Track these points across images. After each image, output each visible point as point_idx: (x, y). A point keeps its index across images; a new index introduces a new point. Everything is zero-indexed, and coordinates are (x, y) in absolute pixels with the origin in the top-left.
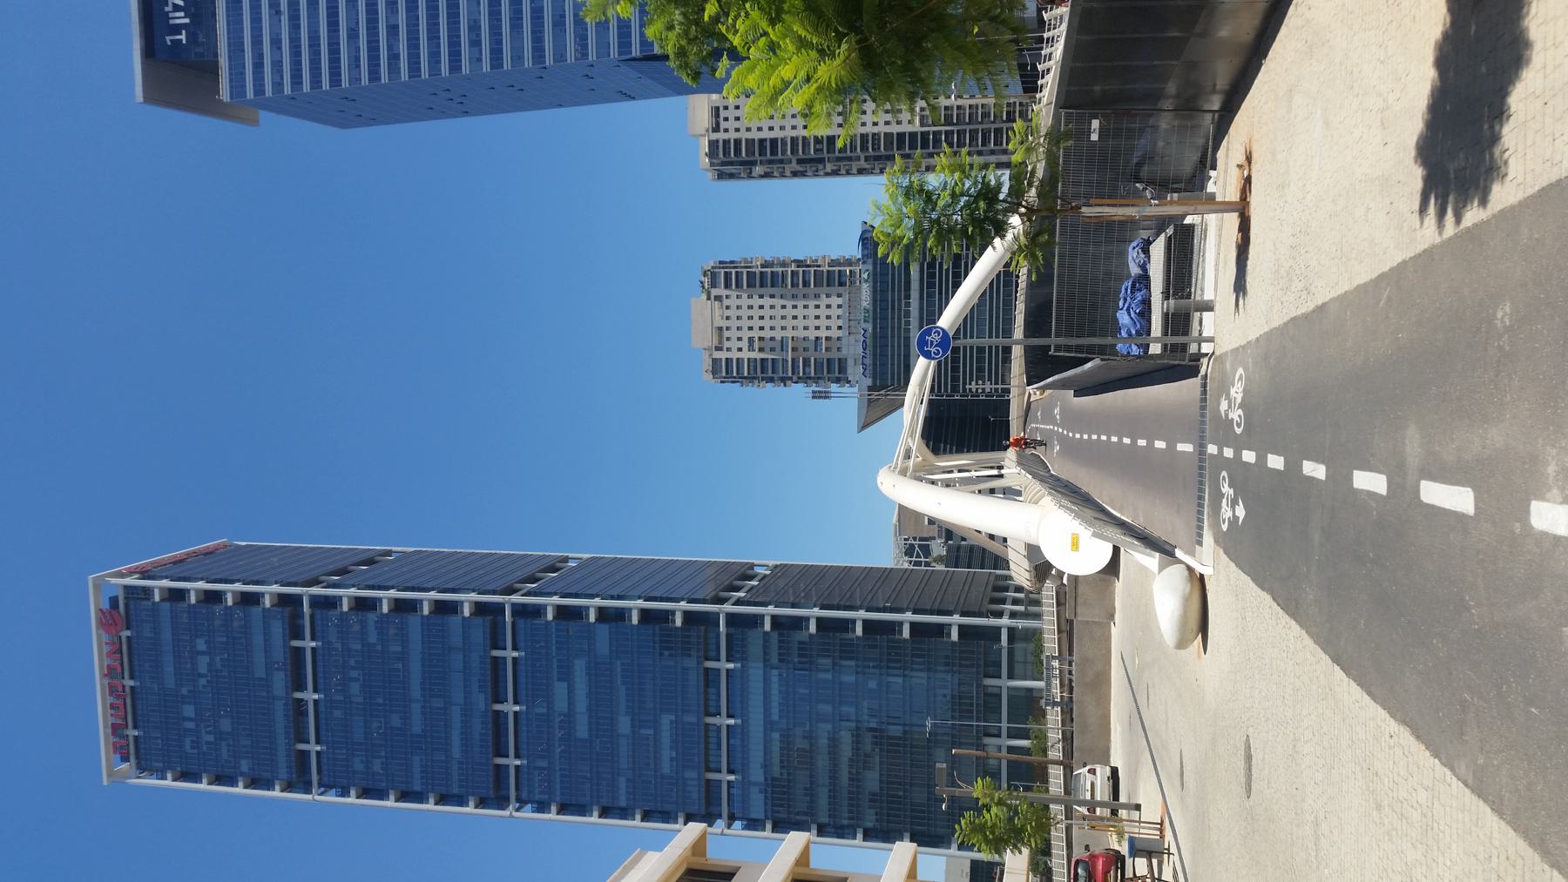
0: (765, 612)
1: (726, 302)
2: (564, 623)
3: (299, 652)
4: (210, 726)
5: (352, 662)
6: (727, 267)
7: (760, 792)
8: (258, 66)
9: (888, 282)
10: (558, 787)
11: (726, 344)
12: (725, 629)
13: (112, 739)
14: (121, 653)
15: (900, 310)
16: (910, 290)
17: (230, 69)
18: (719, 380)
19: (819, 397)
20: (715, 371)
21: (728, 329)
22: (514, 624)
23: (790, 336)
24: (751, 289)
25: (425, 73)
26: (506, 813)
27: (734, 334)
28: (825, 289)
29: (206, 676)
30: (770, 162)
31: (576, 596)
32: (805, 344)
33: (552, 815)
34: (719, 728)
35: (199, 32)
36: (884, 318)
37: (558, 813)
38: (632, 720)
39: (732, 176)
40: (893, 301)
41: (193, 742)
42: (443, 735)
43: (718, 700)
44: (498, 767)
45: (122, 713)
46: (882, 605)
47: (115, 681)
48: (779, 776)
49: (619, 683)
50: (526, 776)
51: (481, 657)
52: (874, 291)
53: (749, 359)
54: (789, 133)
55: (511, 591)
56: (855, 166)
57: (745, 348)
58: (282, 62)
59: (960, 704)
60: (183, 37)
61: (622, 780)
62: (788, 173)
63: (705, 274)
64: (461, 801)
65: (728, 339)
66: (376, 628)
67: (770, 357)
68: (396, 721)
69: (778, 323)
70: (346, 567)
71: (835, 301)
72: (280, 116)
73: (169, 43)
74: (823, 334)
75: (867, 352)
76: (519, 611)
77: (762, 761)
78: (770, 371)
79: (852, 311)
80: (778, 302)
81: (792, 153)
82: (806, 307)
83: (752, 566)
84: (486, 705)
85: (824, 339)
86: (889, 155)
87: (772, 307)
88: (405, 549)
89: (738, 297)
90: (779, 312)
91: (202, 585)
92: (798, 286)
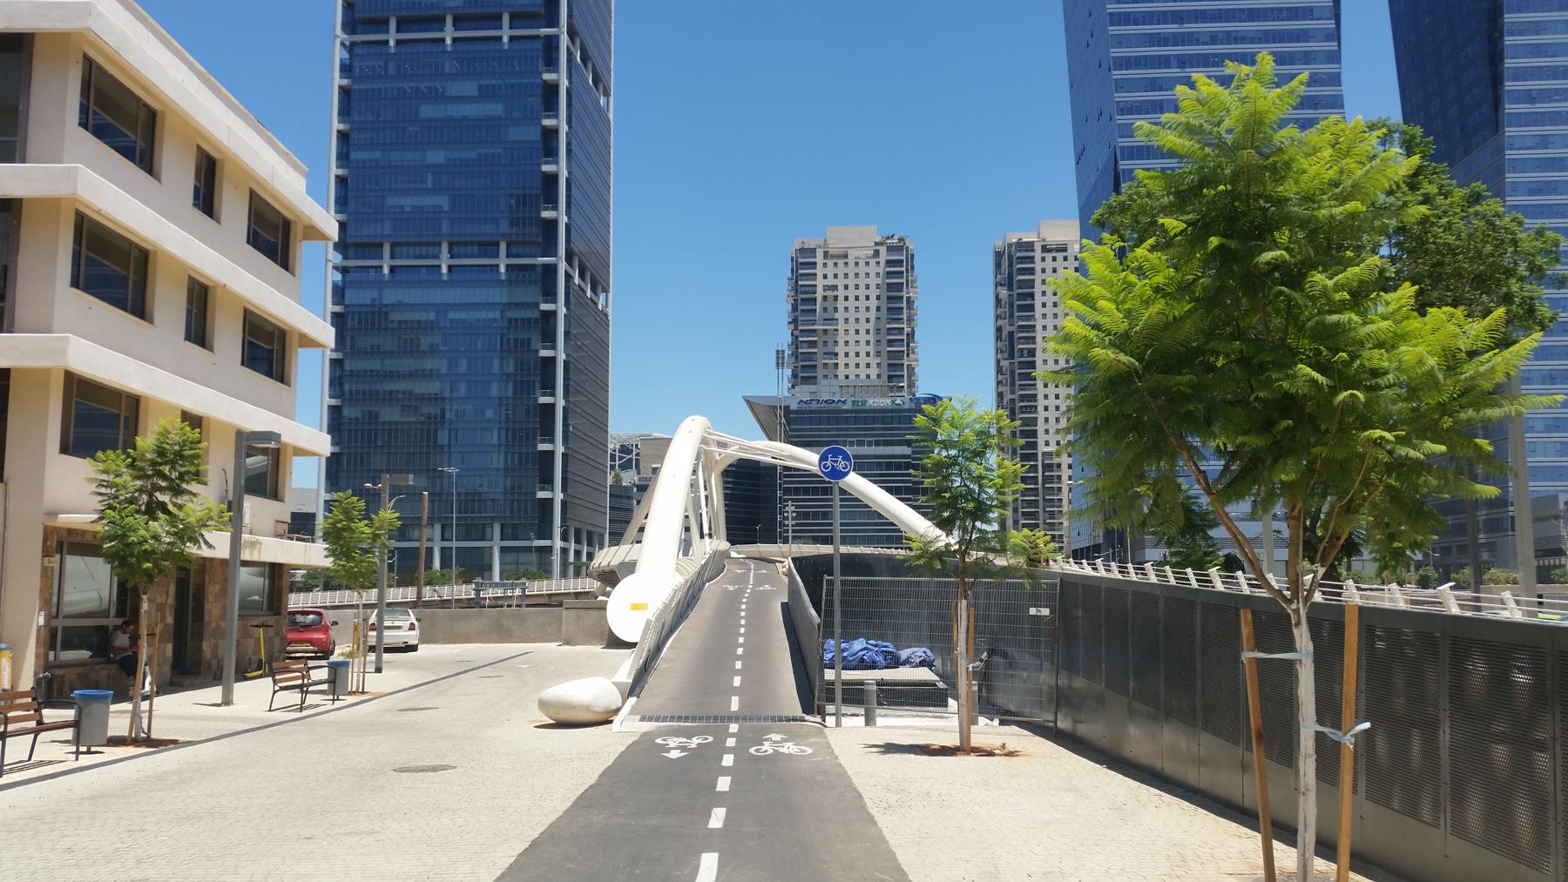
0: (559, 304)
1: (873, 262)
2: (540, 92)
6: (907, 262)
11: (830, 263)
15: (865, 436)
19: (778, 358)
20: (803, 251)
21: (846, 264)
22: (537, 37)
23: (839, 328)
26: (339, 31)
27: (841, 270)
28: (885, 362)
30: (1011, 305)
31: (569, 105)
32: (831, 343)
33: (338, 81)
34: (436, 257)
38: (441, 165)
39: (998, 265)
43: (467, 256)
44: (386, 22)
49: (480, 151)
52: (883, 411)
55: (572, 34)
56: (1005, 389)
59: (473, 501)
61: (377, 155)
62: (1000, 322)
63: (901, 240)
65: (836, 264)
67: (818, 307)
71: (874, 372)
74: (841, 361)
75: (824, 405)
79: (871, 389)
80: (873, 315)
82: (868, 343)
83: (606, 290)
84: (451, 8)
87: (868, 309)
89: (878, 274)
90: (863, 316)
92: (888, 334)
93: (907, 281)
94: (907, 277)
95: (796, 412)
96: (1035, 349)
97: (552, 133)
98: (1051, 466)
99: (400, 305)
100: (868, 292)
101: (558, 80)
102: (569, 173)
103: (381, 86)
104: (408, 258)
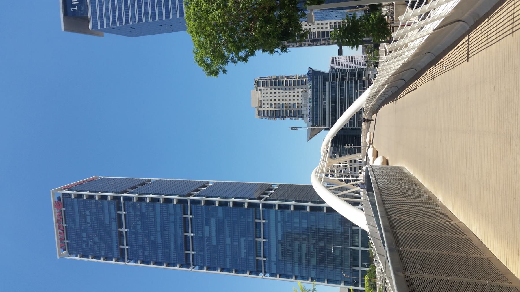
0: (276, 203)
1: (263, 91)
2: (208, 206)
3: (120, 215)
4: (91, 240)
5: (137, 219)
6: (263, 79)
7: (275, 264)
8: (102, 17)
10: (206, 261)
11: (263, 106)
12: (262, 209)
13: (60, 244)
14: (62, 215)
15: (322, 98)
17: (92, 19)
19: (294, 129)
21: (263, 100)
22: (191, 206)
23: (285, 103)
25: (157, 19)
26: (189, 269)
27: (265, 102)
29: (89, 223)
32: (290, 105)
33: (205, 271)
34: (260, 242)
35: (82, 7)
36: (316, 101)
37: (207, 270)
38: (231, 239)
40: (319, 95)
41: (86, 245)
42: (168, 241)
43: (260, 233)
44: (187, 254)
45: (63, 235)
46: (316, 201)
47: (61, 225)
48: (281, 259)
49: (226, 226)
50: (196, 259)
51: (180, 217)
52: (313, 92)
53: (271, 111)
55: (189, 195)
56: (307, 43)
58: (109, 16)
59: (344, 235)
60: (76, 8)
61: (228, 259)
63: (255, 82)
64: (175, 265)
65: (264, 104)
66: (145, 207)
67: (278, 110)
68: (152, 238)
69: (281, 98)
70: (136, 186)
72: (110, 34)
73: (72, 11)
74: (296, 102)
75: (310, 113)
76: (192, 202)
79: (305, 99)
80: (281, 91)
82: (290, 92)
83: (271, 185)
84: (182, 234)
85: (296, 103)
87: (279, 93)
88: (155, 179)
89: (267, 90)
90: (281, 94)
91: (87, 193)
93: (269, 79)
94: (268, 79)
95: (313, 123)
97: (220, 203)
101: (204, 200)
102: (233, 198)
103: (206, 257)
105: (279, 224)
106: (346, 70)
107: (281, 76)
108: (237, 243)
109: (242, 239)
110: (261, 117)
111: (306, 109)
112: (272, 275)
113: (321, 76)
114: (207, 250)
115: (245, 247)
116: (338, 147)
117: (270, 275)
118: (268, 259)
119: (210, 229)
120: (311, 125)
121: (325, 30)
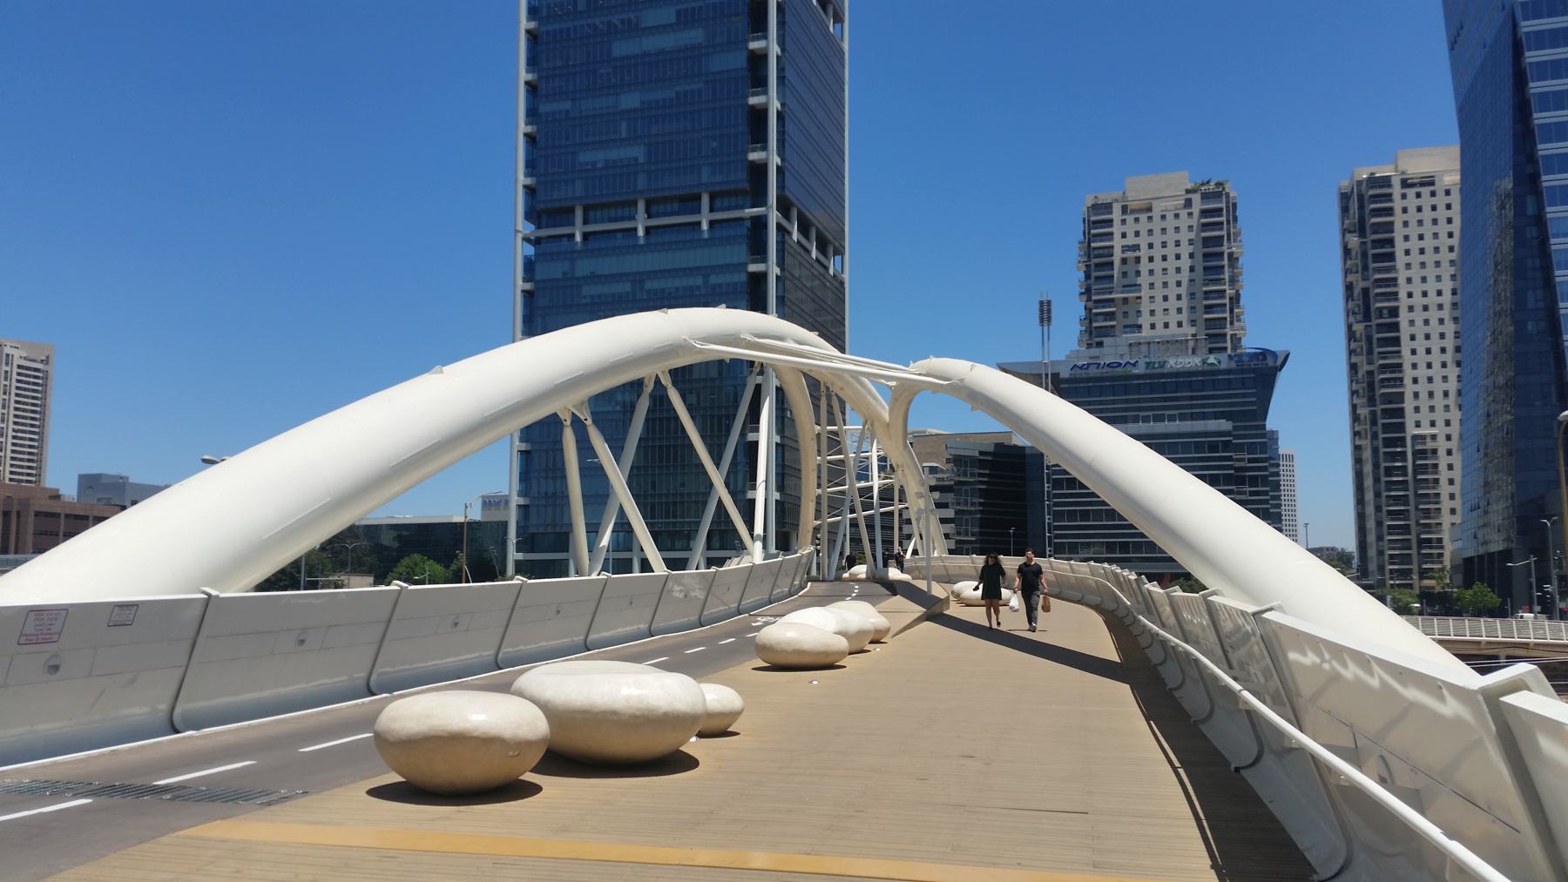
0: (770, 263)
1: (1184, 213)
6: (1228, 211)
7: (565, 273)
9: (1202, 391)
10: (557, 27)
11: (1130, 218)
16: (1192, 419)
18: (1086, 216)
19: (1042, 311)
20: (1096, 208)
21: (1150, 218)
23: (1142, 294)
24: (1201, 242)
27: (1143, 226)
30: (1364, 255)
31: (781, 23)
32: (1132, 314)
34: (633, 218)
36: (1152, 388)
38: (635, 110)
39: (1345, 210)
40: (1176, 399)
49: (678, 88)
52: (1189, 373)
53: (1112, 247)
54: (1402, 276)
57: (1126, 242)
59: (675, 503)
61: (567, 105)
62: (1351, 278)
63: (1219, 184)
67: (1116, 272)
75: (1106, 369)
77: (599, 273)
78: (1098, 274)
80: (1185, 276)
81: (1380, 365)
82: (1179, 311)
83: (839, 252)
86: (1375, 400)
89: (1191, 227)
90: (1172, 278)
92: (1206, 299)
93: (1229, 235)
95: (1067, 381)
96: (1397, 308)
97: (760, 59)
98: (1424, 452)
99: (593, 278)
100: (1178, 250)
102: (783, 105)
104: (602, 221)
105: (699, 281)
106: (1279, 502)
107: (1241, 274)
108: (624, 135)
109: (638, 152)
110: (1089, 217)
111: (1122, 355)
112: (529, 266)
113: (1254, 399)
114: (595, 24)
115: (615, 161)
116: (980, 475)
117: (531, 260)
118: (579, 247)
119: (664, 26)
120: (1059, 374)
121: (1410, 418)
